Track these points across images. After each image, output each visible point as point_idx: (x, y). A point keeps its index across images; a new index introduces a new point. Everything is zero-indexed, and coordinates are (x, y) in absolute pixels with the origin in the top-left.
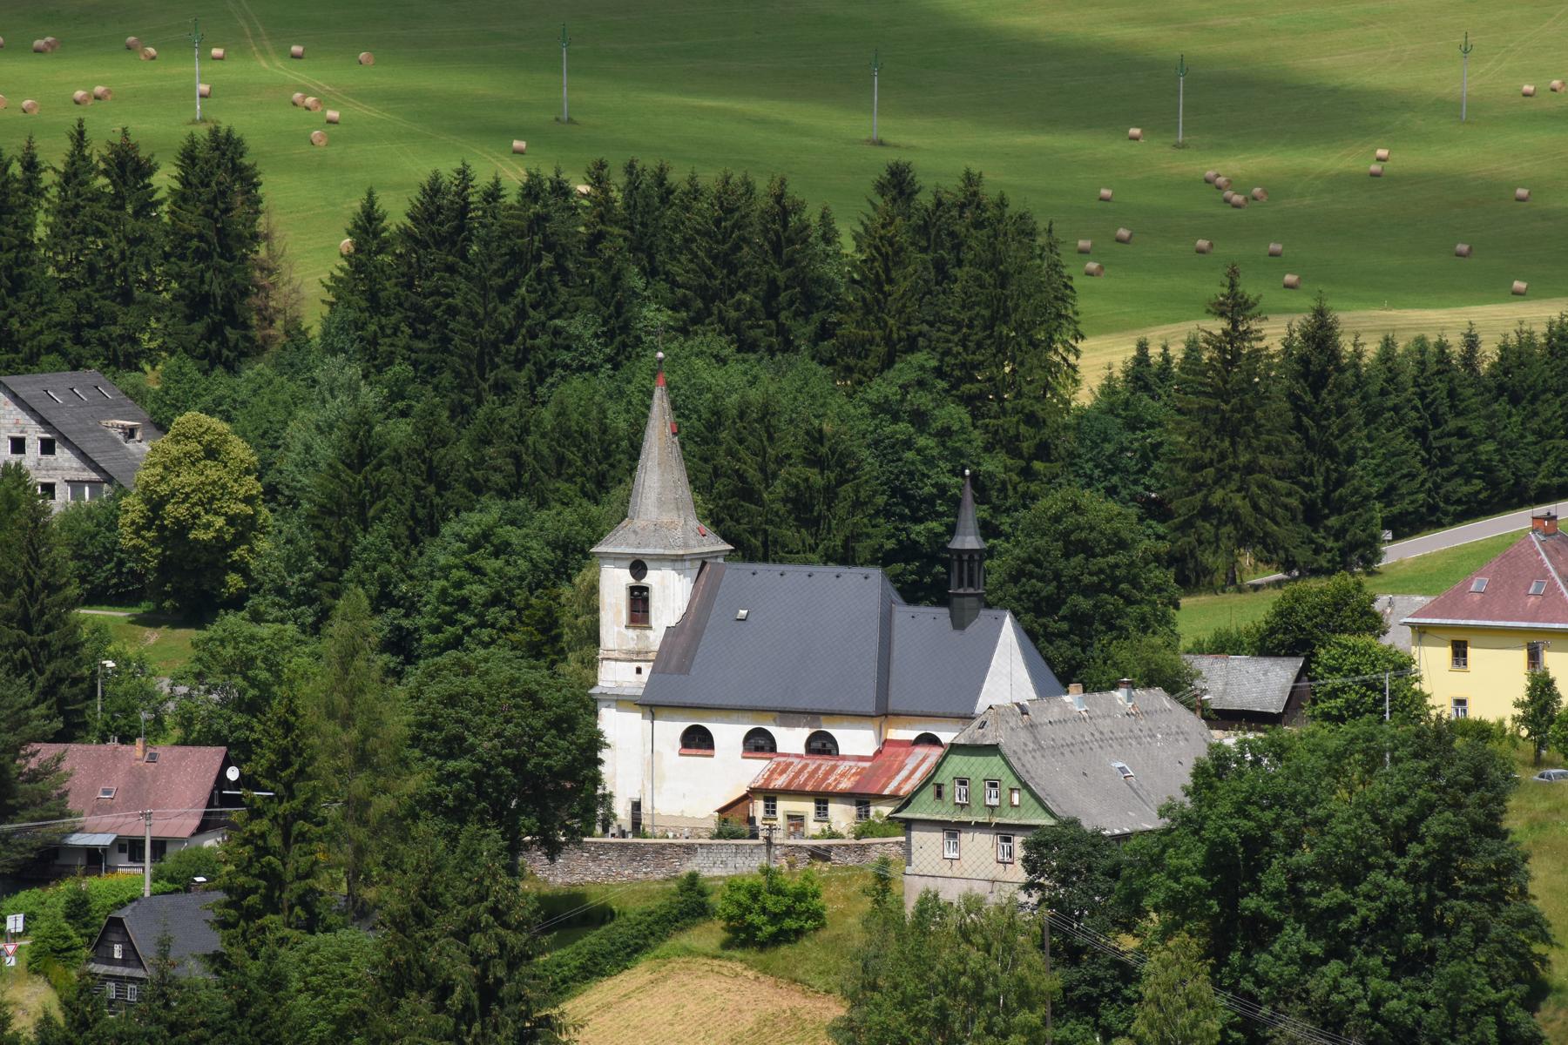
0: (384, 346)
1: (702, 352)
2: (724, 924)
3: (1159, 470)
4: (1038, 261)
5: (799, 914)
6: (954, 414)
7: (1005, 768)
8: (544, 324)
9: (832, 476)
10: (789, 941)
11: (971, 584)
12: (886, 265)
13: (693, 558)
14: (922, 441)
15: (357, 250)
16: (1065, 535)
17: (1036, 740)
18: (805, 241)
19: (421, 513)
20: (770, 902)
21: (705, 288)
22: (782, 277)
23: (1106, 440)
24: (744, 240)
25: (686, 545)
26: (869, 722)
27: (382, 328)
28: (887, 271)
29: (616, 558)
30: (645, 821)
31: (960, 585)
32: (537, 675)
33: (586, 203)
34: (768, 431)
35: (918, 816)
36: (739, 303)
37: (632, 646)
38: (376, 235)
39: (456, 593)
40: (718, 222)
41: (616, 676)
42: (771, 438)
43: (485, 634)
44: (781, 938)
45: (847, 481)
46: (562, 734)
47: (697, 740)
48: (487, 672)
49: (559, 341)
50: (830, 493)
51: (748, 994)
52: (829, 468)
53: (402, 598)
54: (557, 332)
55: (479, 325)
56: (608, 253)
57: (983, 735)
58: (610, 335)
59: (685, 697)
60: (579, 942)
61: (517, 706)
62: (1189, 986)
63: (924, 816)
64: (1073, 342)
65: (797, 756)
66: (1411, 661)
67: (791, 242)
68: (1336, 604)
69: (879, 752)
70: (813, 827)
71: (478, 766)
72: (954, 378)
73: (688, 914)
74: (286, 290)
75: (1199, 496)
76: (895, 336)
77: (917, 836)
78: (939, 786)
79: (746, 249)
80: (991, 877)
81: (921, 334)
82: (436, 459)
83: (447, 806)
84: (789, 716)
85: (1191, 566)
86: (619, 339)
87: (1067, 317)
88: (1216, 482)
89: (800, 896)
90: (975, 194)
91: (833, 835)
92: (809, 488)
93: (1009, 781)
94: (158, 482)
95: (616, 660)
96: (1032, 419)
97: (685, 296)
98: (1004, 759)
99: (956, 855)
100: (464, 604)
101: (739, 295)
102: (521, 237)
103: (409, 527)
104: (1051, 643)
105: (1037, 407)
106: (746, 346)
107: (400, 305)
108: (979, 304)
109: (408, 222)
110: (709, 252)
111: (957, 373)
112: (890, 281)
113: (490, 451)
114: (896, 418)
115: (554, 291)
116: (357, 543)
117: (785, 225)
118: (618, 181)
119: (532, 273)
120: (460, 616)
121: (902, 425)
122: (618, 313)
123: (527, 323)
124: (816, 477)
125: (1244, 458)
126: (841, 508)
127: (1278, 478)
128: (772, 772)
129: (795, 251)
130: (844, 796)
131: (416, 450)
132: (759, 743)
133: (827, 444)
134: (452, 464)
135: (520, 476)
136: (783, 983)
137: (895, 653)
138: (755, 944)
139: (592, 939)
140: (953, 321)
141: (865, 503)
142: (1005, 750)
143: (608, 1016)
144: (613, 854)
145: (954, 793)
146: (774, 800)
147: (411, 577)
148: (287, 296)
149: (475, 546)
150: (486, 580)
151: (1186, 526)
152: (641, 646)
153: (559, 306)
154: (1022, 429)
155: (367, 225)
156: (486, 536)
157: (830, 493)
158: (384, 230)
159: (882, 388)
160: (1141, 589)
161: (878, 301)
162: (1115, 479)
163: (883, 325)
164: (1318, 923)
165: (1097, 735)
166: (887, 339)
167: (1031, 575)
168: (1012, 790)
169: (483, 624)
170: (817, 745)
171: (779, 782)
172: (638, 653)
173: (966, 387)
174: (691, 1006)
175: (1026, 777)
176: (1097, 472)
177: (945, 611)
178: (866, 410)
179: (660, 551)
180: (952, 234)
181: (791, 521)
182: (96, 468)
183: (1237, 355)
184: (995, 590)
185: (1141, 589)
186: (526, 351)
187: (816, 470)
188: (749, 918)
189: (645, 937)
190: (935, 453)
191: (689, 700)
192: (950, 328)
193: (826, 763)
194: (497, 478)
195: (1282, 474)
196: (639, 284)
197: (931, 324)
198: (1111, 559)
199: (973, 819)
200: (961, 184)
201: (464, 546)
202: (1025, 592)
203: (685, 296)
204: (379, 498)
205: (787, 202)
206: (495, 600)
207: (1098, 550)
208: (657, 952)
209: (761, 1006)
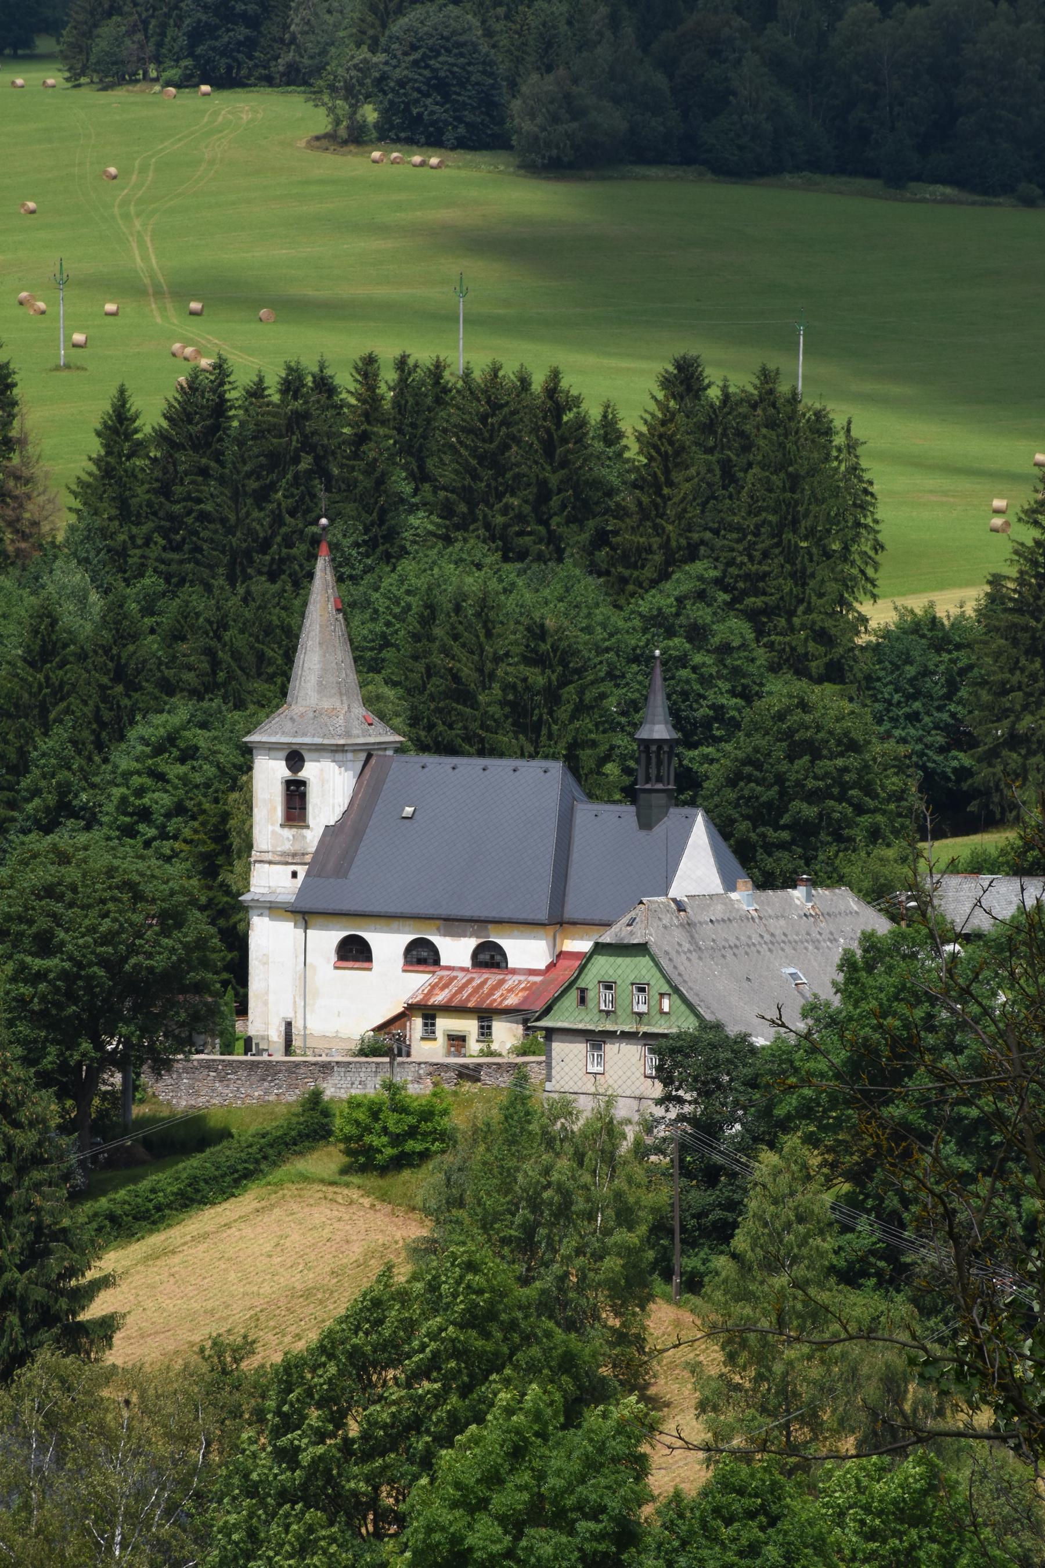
0: (135, 557)
1: (462, 560)
2: (342, 1146)
3: (966, 696)
4: (835, 464)
5: (425, 1134)
6: (735, 628)
7: (654, 970)
8: (302, 532)
9: (554, 677)
10: (411, 1165)
11: (659, 779)
12: (666, 466)
13: (356, 749)
14: (698, 659)
15: (109, 453)
16: (789, 734)
17: (692, 939)
18: (579, 441)
19: (107, 716)
20: (391, 1120)
21: (469, 490)
22: (554, 481)
23: (909, 661)
24: (514, 438)
25: (348, 734)
26: (541, 931)
27: (132, 538)
29: (271, 748)
30: (297, 1042)
31: (648, 780)
32: (141, 865)
33: (353, 401)
34: (485, 626)
36: (506, 510)
37: (287, 847)
38: (128, 437)
39: (137, 802)
40: (484, 419)
41: (270, 880)
42: (489, 634)
43: (166, 846)
44: (402, 1162)
45: (571, 682)
47: (354, 952)
48: (85, 861)
50: (552, 696)
51: (360, 1223)
52: (551, 666)
53: (82, 808)
55: (230, 531)
56: (372, 454)
57: (632, 933)
58: (372, 544)
59: (339, 905)
60: (181, 1166)
61: (114, 899)
62: (799, 1197)
63: (566, 1025)
64: (871, 553)
65: (462, 969)
67: (564, 440)
69: (552, 966)
70: (474, 1046)
71: (67, 965)
72: (737, 590)
73: (308, 1136)
74: (42, 499)
75: (1006, 723)
76: (674, 544)
77: (558, 1048)
78: (583, 991)
79: (515, 448)
80: (637, 1094)
81: (702, 542)
82: (124, 655)
83: (33, 1012)
84: (455, 924)
85: (996, 799)
86: (381, 548)
87: (866, 526)
88: (1025, 707)
89: (427, 1114)
90: (771, 392)
91: (491, 1054)
92: (528, 689)
95: (270, 863)
96: (823, 637)
97: (447, 499)
98: (653, 960)
99: (600, 1069)
100: (145, 815)
101: (508, 499)
102: (281, 436)
103: (93, 731)
104: (770, 855)
105: (829, 623)
106: (510, 553)
107: (155, 514)
108: (765, 509)
109: (165, 424)
110: (473, 452)
111: (741, 585)
112: (670, 484)
113: (184, 647)
114: (670, 633)
115: (313, 496)
116: (36, 749)
117: (558, 422)
118: (389, 375)
119: (289, 476)
120: (142, 827)
121: (676, 640)
122: (382, 521)
123: (284, 530)
124: (538, 678)
126: (563, 713)
128: (433, 987)
129: (568, 451)
130: (507, 1013)
131: (103, 647)
132: (421, 955)
133: (549, 641)
134: (145, 661)
135: (214, 673)
136: (401, 1211)
137: (575, 856)
138: (376, 1168)
139: (193, 1164)
140: (739, 529)
141: (592, 707)
142: (654, 949)
143: (202, 1247)
144: (243, 1074)
145: (600, 999)
146: (434, 1017)
147: (93, 786)
148: (42, 508)
149: (159, 750)
150: (169, 787)
151: (993, 754)
152: (297, 847)
154: (812, 646)
155: (119, 424)
156: (172, 739)
157: (552, 696)
158: (136, 431)
159: (659, 600)
160: (875, 796)
161: (656, 507)
162: (917, 705)
163: (658, 530)
164: (967, 1135)
165: (767, 937)
166: (666, 545)
167: (749, 779)
168: (662, 995)
169: (164, 836)
170: (484, 957)
171: (440, 998)
172: (294, 855)
173: (750, 601)
174: (295, 1237)
175: (677, 980)
176: (897, 697)
177: (632, 809)
178: (637, 623)
179: (318, 740)
180: (741, 434)
181: (508, 725)
184: (712, 796)
185: (875, 796)
186: (282, 561)
187: (537, 670)
188: (368, 1139)
189: (257, 1162)
190: (714, 670)
191: (346, 907)
192: (735, 536)
193: (492, 977)
194: (189, 677)
196: (408, 489)
197: (716, 532)
198: (840, 762)
199: (619, 1028)
200: (757, 382)
201: (148, 749)
203: (447, 499)
204: (62, 699)
205: (561, 398)
206: (179, 809)
207: (825, 752)
208: (270, 1178)
209: (373, 1236)
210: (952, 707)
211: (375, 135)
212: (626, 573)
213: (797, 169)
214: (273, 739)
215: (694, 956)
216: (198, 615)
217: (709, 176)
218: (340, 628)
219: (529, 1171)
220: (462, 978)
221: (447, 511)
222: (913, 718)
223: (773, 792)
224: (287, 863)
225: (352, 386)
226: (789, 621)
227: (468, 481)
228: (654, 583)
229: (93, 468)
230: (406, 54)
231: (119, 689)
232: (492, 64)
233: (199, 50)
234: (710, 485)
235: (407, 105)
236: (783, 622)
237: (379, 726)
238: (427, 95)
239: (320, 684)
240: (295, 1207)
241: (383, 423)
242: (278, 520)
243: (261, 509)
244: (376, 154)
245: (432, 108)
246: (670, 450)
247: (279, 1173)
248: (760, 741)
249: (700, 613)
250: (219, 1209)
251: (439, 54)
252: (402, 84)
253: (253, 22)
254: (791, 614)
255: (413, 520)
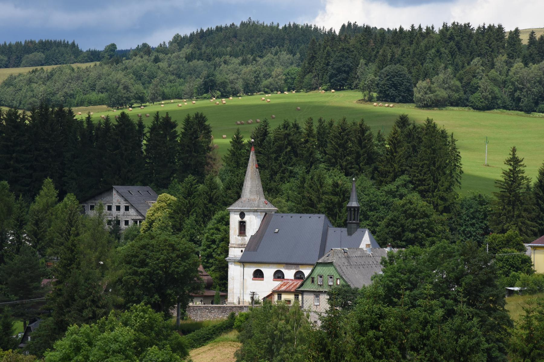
7: (335, 271)
9: (340, 200)
11: (354, 220)
13: (261, 211)
16: (405, 212)
17: (349, 262)
22: (361, 152)
25: (258, 206)
28: (395, 148)
29: (235, 211)
31: (351, 220)
33: (304, 131)
35: (306, 289)
36: (347, 160)
37: (240, 242)
40: (340, 133)
41: (235, 253)
42: (321, 186)
46: (183, 260)
47: (258, 275)
49: (292, 175)
53: (198, 241)
54: (291, 172)
63: (308, 289)
64: (459, 174)
65: (291, 280)
66: (530, 258)
68: (507, 240)
72: (416, 185)
75: (501, 226)
76: (397, 170)
78: (313, 278)
84: (289, 265)
87: (458, 166)
93: (336, 276)
94: (152, 216)
95: (234, 247)
100: (214, 242)
103: (202, 218)
110: (337, 143)
111: (417, 183)
112: (396, 152)
118: (316, 124)
120: (212, 246)
123: (282, 169)
124: (336, 199)
125: (516, 213)
127: (529, 220)
128: (281, 285)
129: (366, 143)
132: (279, 275)
134: (218, 197)
140: (418, 166)
142: (335, 264)
145: (319, 281)
146: (281, 295)
152: (243, 242)
153: (292, 163)
154: (439, 201)
159: (392, 187)
161: (391, 159)
162: (474, 221)
165: (375, 262)
167: (392, 225)
168: (337, 279)
170: (298, 276)
171: (283, 288)
172: (242, 245)
175: (342, 274)
176: (467, 218)
177: (346, 229)
178: (384, 193)
179: (249, 208)
182: (142, 215)
183: (515, 178)
189: (212, 335)
195: (532, 220)
198: (421, 220)
199: (323, 290)
202: (390, 231)
210: (485, 222)
211: (376, 99)
212: (382, 179)
213: (499, 108)
214: (236, 208)
215: (349, 267)
216: (234, 182)
217: (472, 110)
218: (257, 173)
219: (269, 326)
220: (291, 282)
221: (329, 160)
222: (473, 225)
223: (400, 229)
224: (240, 248)
225: (305, 127)
226: (433, 194)
227: (335, 152)
228: (391, 182)
229: (229, 153)
230: (385, 77)
231: (211, 204)
232: (410, 80)
233: (332, 81)
234: (409, 152)
235: (385, 91)
236: (431, 194)
237: (270, 205)
238: (391, 88)
239: (250, 191)
240: (221, 348)
241: (313, 137)
242: (281, 166)
243: (276, 163)
244: (375, 104)
245: (392, 92)
246: (396, 142)
247: (218, 339)
248: (395, 213)
249: (403, 191)
250: (198, 349)
251: (394, 77)
252: (384, 85)
253: (348, 73)
254: (433, 191)
255: (320, 165)
